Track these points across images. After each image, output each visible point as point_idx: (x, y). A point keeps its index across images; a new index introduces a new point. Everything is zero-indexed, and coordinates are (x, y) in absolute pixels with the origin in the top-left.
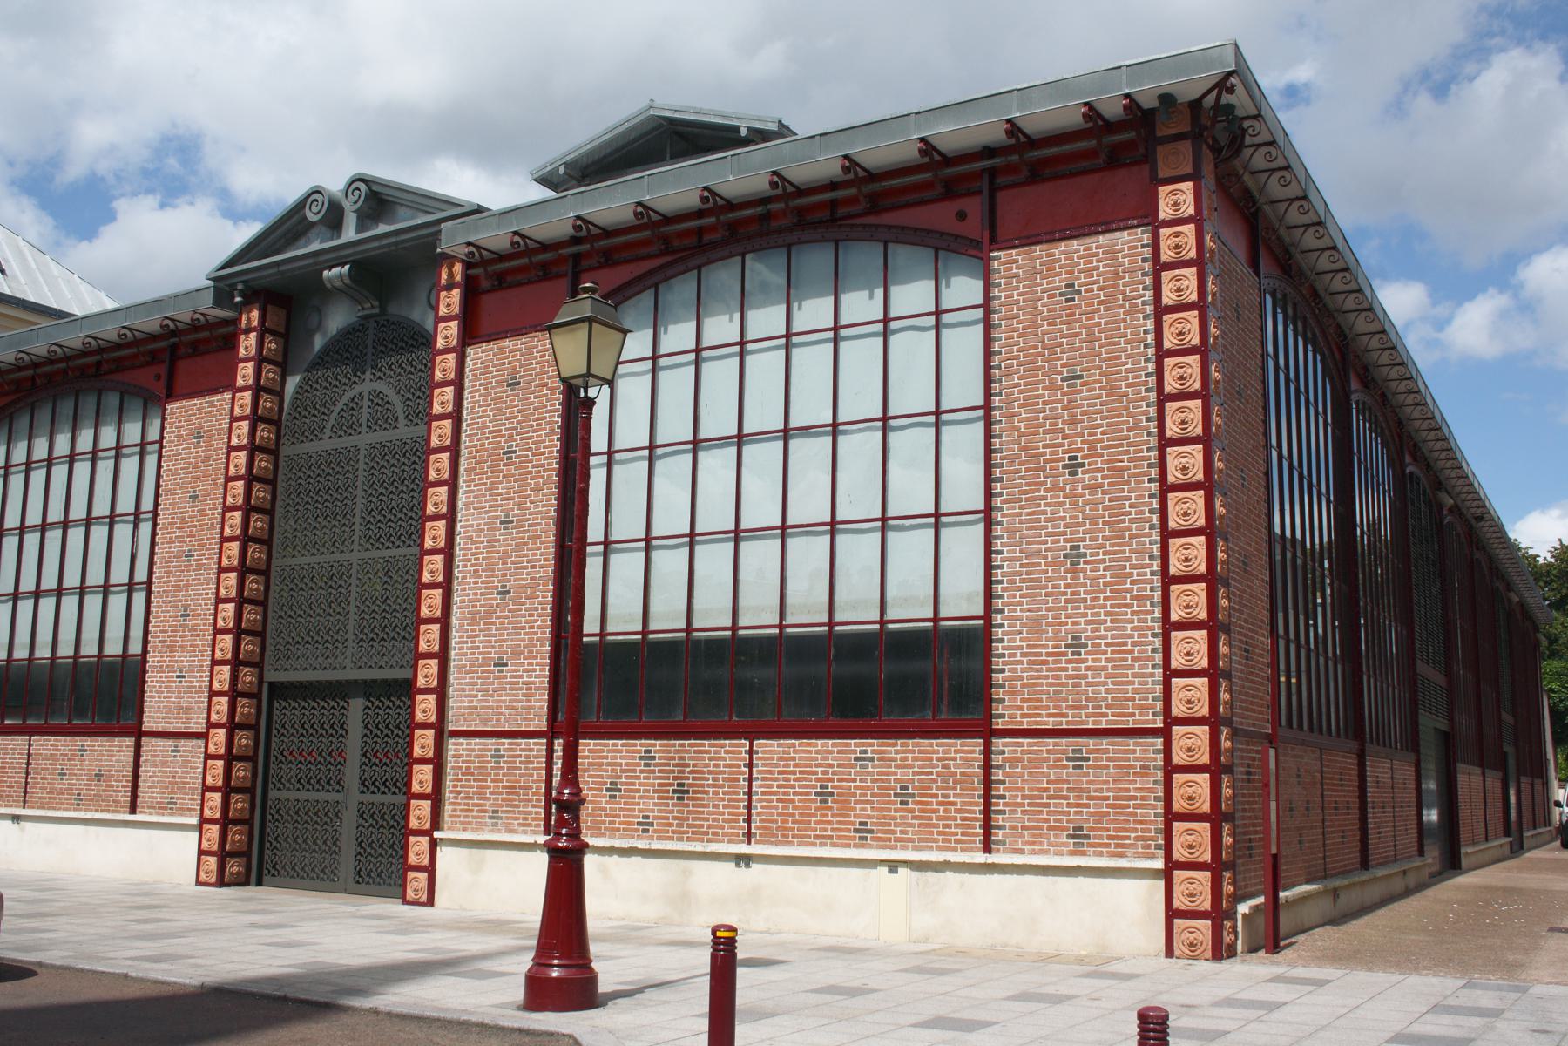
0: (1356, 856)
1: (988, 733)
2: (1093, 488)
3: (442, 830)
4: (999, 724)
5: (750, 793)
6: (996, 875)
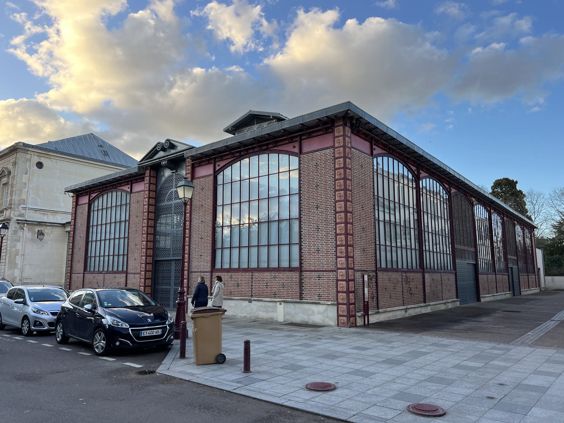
5: (252, 285)
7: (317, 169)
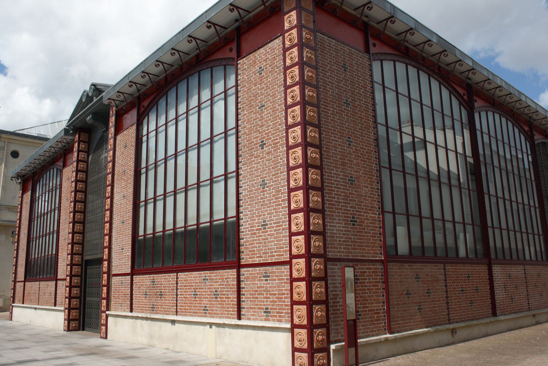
0: (490, 311)
1: (239, 266)
2: (268, 153)
3: (110, 310)
4: (243, 262)
6: (240, 330)
7: (261, 79)
